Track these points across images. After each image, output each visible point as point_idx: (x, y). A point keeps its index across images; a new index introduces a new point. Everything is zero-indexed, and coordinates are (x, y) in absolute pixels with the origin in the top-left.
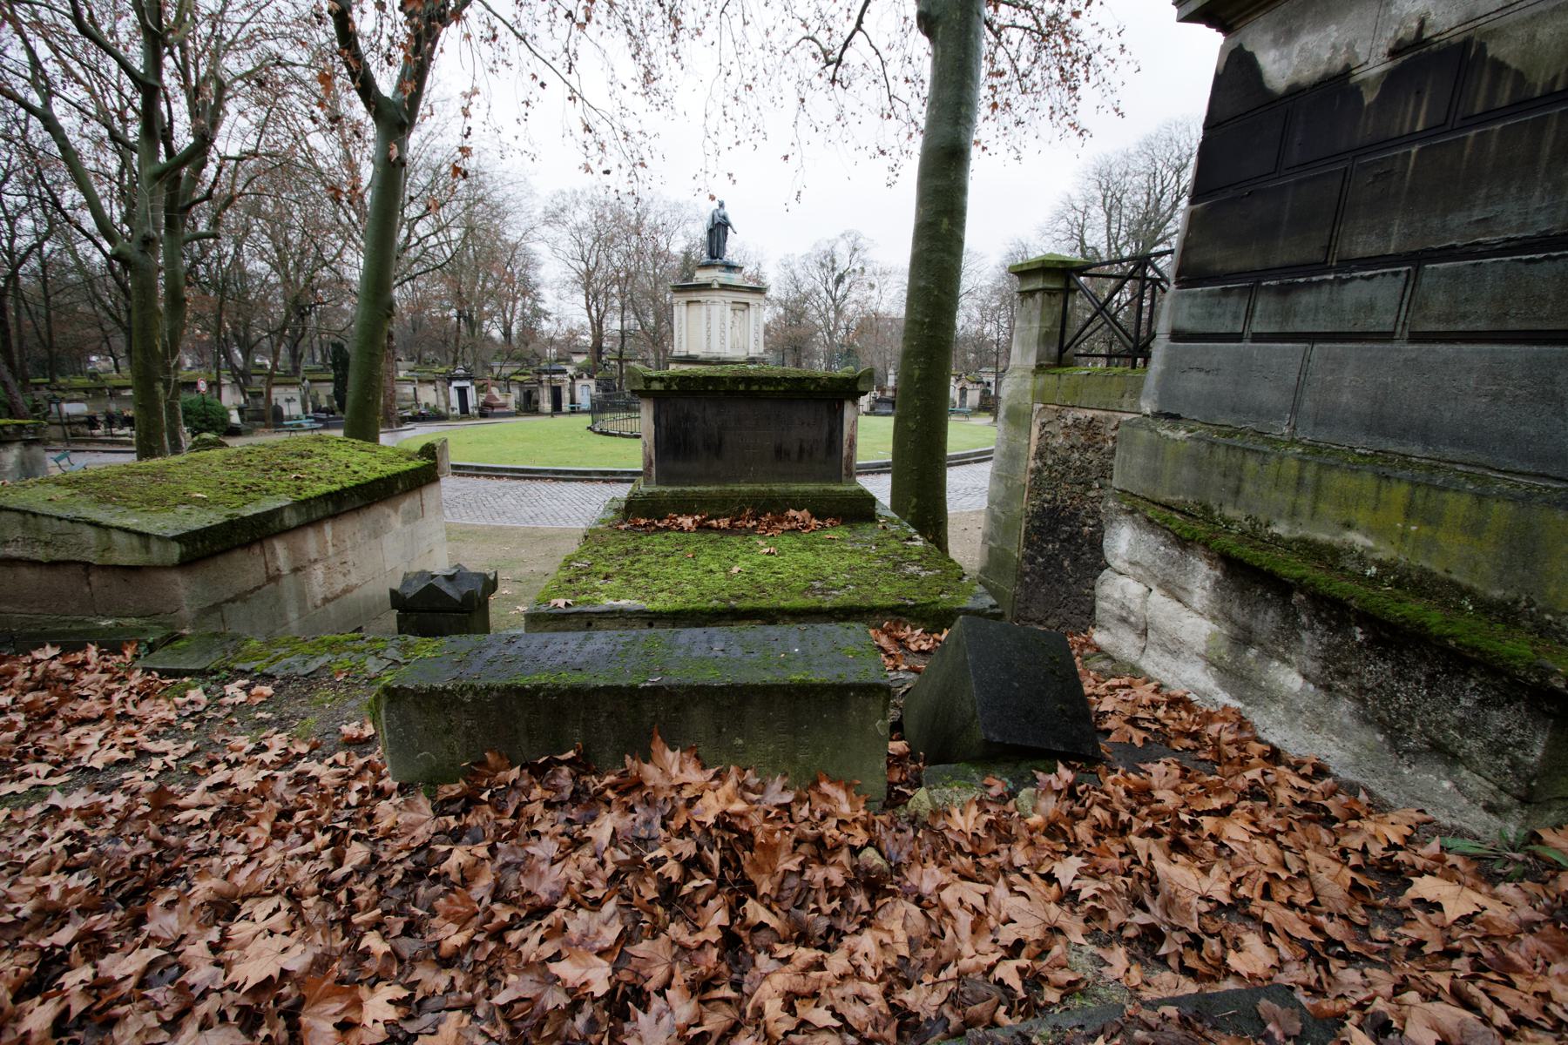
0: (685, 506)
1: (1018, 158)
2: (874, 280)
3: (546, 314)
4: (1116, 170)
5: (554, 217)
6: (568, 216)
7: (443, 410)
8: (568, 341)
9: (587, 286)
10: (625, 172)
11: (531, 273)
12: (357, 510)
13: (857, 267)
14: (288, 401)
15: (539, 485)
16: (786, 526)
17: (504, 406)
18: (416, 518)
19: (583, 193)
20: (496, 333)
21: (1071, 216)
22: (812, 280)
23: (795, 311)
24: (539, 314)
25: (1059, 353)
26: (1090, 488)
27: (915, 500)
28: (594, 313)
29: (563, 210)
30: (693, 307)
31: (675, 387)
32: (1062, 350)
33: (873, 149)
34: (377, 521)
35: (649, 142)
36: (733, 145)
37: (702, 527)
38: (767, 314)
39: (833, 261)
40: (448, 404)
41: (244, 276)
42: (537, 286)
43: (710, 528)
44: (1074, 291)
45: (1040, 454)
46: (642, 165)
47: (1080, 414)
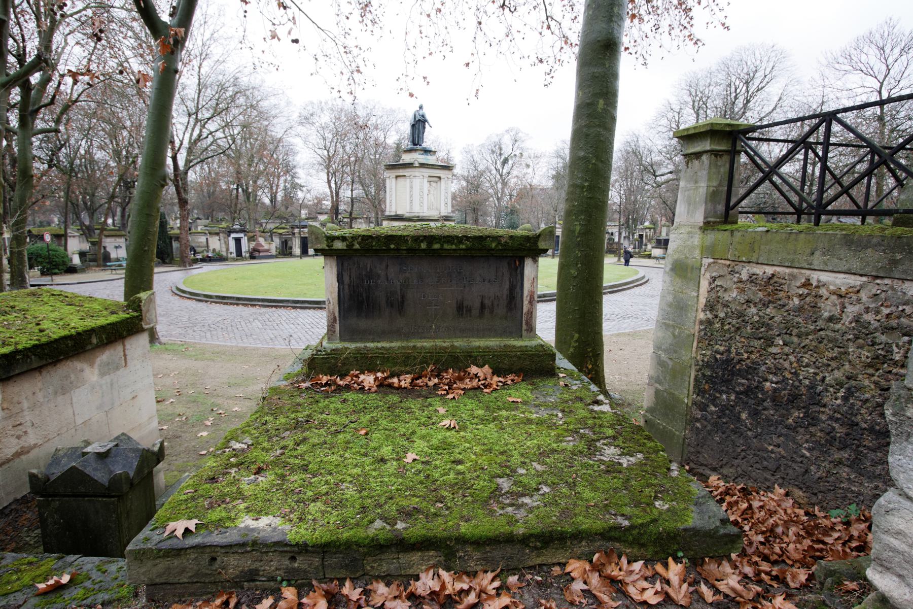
0: (367, 363)
1: (645, 64)
2: (530, 162)
3: (301, 187)
4: (702, 83)
5: (306, 120)
6: (315, 119)
7: (224, 254)
8: (316, 205)
9: (328, 167)
10: (345, 77)
11: (291, 158)
12: (39, 369)
13: (517, 153)
14: (116, 247)
15: (281, 311)
16: (468, 384)
17: (267, 251)
18: (117, 368)
19: (326, 103)
20: (267, 201)
21: (670, 115)
22: (486, 162)
23: (474, 183)
24: (296, 186)
25: (724, 213)
26: (772, 344)
27: (577, 335)
28: (333, 185)
29: (312, 115)
30: (399, 179)
31: (357, 246)
32: (728, 208)
33: (533, 59)
34: (67, 377)
35: (363, 55)
36: (427, 55)
37: (383, 386)
38: (454, 186)
39: (501, 149)
40: (228, 249)
41: (92, 161)
42: (295, 167)
43: (390, 386)
44: (739, 152)
45: (710, 306)
46: (358, 71)
47: (758, 270)
